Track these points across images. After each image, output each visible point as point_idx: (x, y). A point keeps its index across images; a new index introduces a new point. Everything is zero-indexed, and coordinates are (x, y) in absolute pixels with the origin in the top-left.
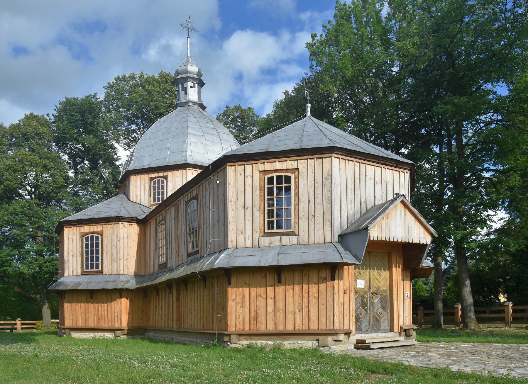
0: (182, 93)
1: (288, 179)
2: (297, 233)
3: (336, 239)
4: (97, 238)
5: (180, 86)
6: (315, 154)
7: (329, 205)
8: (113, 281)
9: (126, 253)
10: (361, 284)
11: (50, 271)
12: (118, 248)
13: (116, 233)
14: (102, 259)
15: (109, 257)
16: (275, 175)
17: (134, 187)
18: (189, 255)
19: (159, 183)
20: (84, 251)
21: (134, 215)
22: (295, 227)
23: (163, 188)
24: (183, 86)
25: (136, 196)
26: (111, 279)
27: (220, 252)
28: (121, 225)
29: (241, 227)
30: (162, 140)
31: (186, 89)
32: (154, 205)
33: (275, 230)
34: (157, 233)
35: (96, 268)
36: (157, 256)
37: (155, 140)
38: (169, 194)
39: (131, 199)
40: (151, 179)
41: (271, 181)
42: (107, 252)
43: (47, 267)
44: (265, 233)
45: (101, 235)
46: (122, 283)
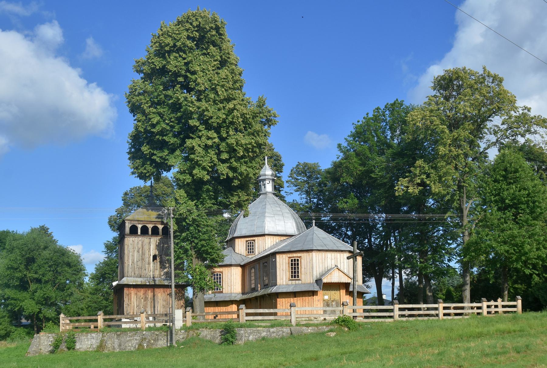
0: (263, 187)
1: (298, 260)
3: (315, 281)
4: (220, 275)
5: (262, 182)
10: (326, 297)
15: (226, 285)
18: (265, 286)
19: (251, 243)
21: (238, 263)
26: (227, 296)
27: (275, 286)
31: (265, 184)
33: (293, 279)
34: (250, 273)
36: (251, 284)
40: (247, 241)
41: (292, 260)
45: (222, 273)
46: (233, 298)
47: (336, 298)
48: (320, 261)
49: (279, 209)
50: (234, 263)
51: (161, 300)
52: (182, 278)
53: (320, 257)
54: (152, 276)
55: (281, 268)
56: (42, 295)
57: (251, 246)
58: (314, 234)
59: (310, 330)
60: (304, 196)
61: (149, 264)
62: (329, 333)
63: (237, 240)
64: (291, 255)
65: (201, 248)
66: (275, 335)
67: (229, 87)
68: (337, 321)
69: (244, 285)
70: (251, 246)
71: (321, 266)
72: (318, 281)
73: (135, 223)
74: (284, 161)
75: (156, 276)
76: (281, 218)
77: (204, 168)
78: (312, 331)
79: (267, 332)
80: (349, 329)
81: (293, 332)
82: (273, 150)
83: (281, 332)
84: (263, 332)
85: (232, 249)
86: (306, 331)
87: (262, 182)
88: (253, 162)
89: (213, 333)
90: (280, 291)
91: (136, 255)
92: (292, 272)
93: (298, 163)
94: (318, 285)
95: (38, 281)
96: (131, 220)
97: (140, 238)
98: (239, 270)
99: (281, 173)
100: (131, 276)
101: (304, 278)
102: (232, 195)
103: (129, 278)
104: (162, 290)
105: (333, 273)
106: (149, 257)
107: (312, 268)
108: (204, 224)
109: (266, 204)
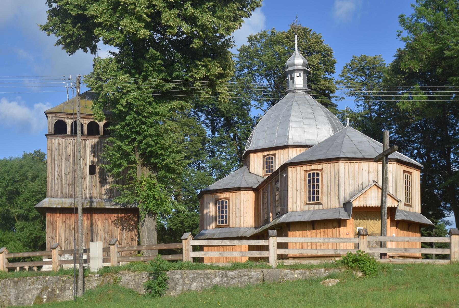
0: (290, 82)
1: (318, 174)
2: (322, 203)
3: (342, 206)
4: (226, 202)
6: (331, 161)
7: (338, 188)
8: (236, 232)
9: (245, 212)
11: (190, 225)
12: (239, 209)
13: (238, 198)
14: (229, 216)
16: (311, 172)
17: (253, 162)
19: (269, 159)
20: (217, 212)
21: (250, 185)
22: (321, 200)
23: (272, 163)
24: (291, 76)
25: (254, 169)
26: (235, 230)
28: (242, 192)
29: (295, 200)
30: (273, 127)
31: (293, 78)
32: (266, 175)
33: (311, 202)
35: (225, 223)
37: (267, 127)
38: (277, 168)
39: (251, 171)
40: (265, 156)
41: (309, 175)
42: (233, 211)
43: (187, 222)
44: (307, 203)
45: (229, 200)
46: (242, 233)
47: (375, 230)
48: (351, 175)
49: (310, 111)
50: (243, 185)
51: (102, 231)
52: (124, 197)
53: (351, 169)
54: (88, 196)
55: (295, 186)
56: (28, 235)
57: (269, 163)
58: (346, 137)
59: (298, 274)
60: (361, 102)
61: (83, 177)
62: (327, 281)
63: (252, 156)
64: (307, 168)
65: (146, 149)
66: (235, 281)
67: (375, 69)
68: (346, 261)
69: (258, 216)
70: (269, 162)
71: (352, 182)
72: (347, 205)
73: (62, 117)
74: (335, 57)
75: (95, 195)
76: (312, 121)
77: (140, 19)
78: (300, 277)
79: (222, 277)
80: (364, 272)
81: (267, 278)
82: (322, 42)
83: (247, 277)
84: (216, 277)
85: (247, 168)
86: (289, 277)
87: (289, 76)
88: (225, 9)
89: (137, 277)
90: (291, 220)
91: (63, 165)
92: (309, 192)
93: (353, 57)
94: (346, 210)
95: (25, 218)
96: (56, 113)
97: (71, 140)
98: (251, 195)
99: (332, 74)
100: (56, 196)
101: (326, 202)
102: (196, 67)
103: (52, 199)
104: (103, 216)
105: (369, 192)
106: (84, 169)
107: (339, 186)
108: (148, 110)
109: (292, 105)
